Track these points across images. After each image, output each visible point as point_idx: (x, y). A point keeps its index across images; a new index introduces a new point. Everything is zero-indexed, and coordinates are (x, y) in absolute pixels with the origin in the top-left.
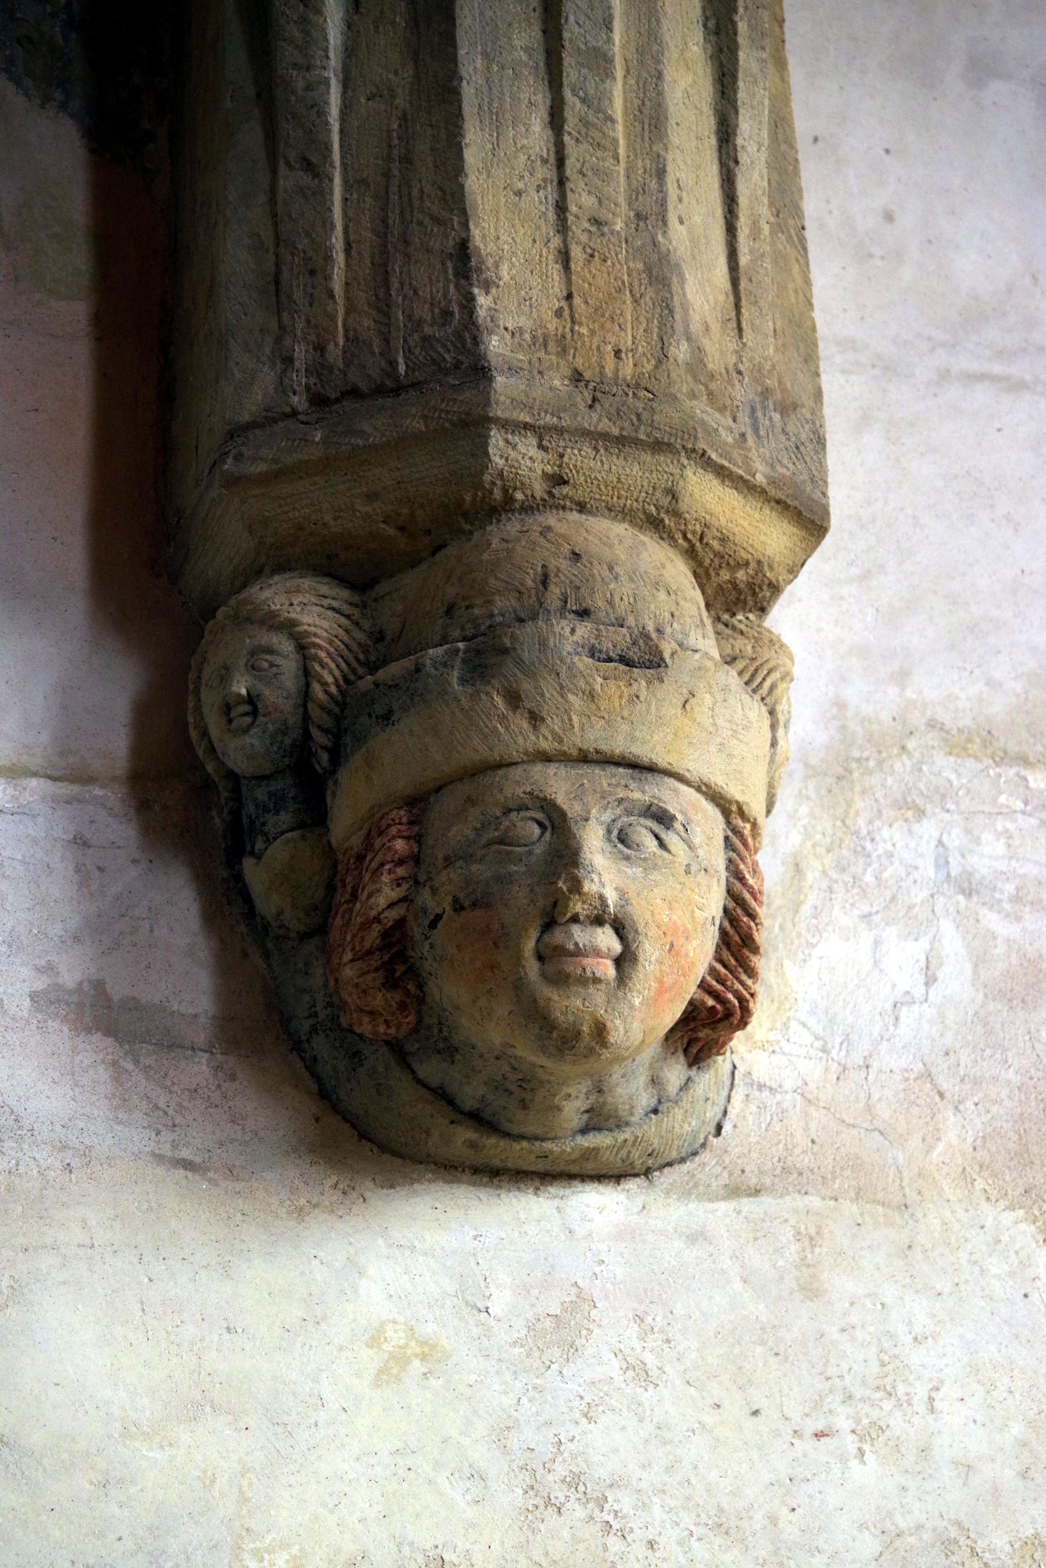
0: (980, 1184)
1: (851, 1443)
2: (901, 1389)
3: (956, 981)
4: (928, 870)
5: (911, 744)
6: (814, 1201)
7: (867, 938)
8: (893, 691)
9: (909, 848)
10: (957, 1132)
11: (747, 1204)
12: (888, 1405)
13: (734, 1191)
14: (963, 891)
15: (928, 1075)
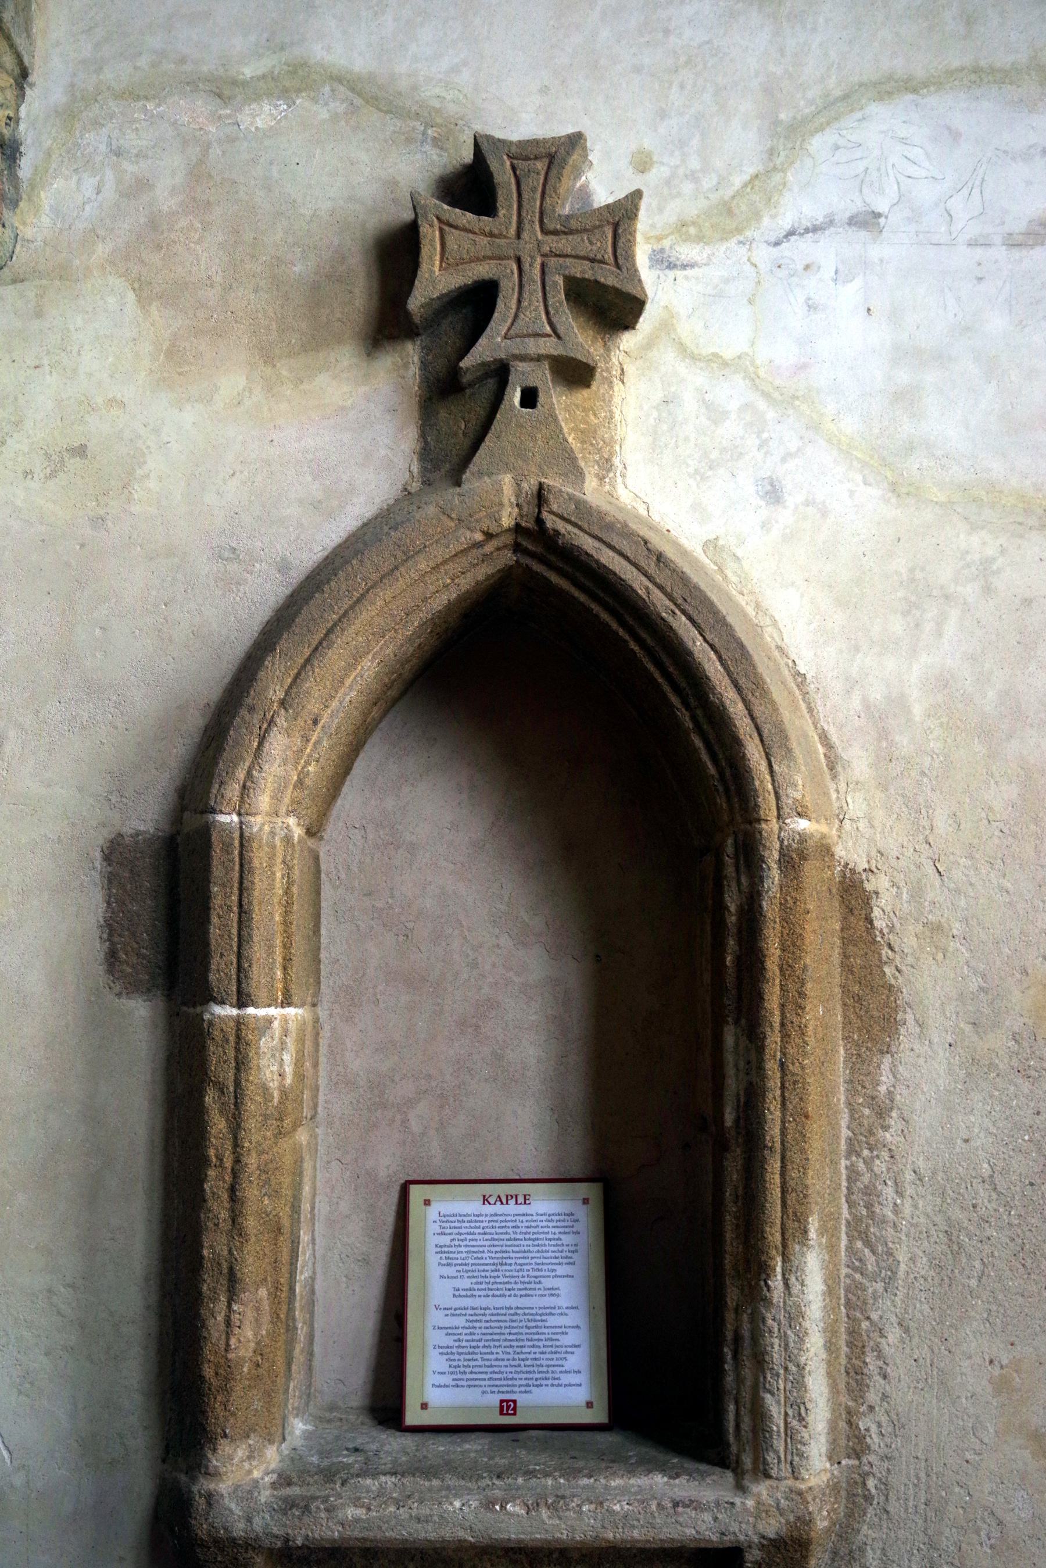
0: (108, 269)
1: (47, 368)
2: (69, 348)
3: (109, 193)
4: (103, 148)
5: (99, 98)
6: (44, 282)
7: (75, 178)
8: (95, 76)
9: (95, 141)
10: (102, 250)
11: (19, 285)
12: (63, 354)
13: (14, 281)
14: (116, 155)
15: (93, 230)
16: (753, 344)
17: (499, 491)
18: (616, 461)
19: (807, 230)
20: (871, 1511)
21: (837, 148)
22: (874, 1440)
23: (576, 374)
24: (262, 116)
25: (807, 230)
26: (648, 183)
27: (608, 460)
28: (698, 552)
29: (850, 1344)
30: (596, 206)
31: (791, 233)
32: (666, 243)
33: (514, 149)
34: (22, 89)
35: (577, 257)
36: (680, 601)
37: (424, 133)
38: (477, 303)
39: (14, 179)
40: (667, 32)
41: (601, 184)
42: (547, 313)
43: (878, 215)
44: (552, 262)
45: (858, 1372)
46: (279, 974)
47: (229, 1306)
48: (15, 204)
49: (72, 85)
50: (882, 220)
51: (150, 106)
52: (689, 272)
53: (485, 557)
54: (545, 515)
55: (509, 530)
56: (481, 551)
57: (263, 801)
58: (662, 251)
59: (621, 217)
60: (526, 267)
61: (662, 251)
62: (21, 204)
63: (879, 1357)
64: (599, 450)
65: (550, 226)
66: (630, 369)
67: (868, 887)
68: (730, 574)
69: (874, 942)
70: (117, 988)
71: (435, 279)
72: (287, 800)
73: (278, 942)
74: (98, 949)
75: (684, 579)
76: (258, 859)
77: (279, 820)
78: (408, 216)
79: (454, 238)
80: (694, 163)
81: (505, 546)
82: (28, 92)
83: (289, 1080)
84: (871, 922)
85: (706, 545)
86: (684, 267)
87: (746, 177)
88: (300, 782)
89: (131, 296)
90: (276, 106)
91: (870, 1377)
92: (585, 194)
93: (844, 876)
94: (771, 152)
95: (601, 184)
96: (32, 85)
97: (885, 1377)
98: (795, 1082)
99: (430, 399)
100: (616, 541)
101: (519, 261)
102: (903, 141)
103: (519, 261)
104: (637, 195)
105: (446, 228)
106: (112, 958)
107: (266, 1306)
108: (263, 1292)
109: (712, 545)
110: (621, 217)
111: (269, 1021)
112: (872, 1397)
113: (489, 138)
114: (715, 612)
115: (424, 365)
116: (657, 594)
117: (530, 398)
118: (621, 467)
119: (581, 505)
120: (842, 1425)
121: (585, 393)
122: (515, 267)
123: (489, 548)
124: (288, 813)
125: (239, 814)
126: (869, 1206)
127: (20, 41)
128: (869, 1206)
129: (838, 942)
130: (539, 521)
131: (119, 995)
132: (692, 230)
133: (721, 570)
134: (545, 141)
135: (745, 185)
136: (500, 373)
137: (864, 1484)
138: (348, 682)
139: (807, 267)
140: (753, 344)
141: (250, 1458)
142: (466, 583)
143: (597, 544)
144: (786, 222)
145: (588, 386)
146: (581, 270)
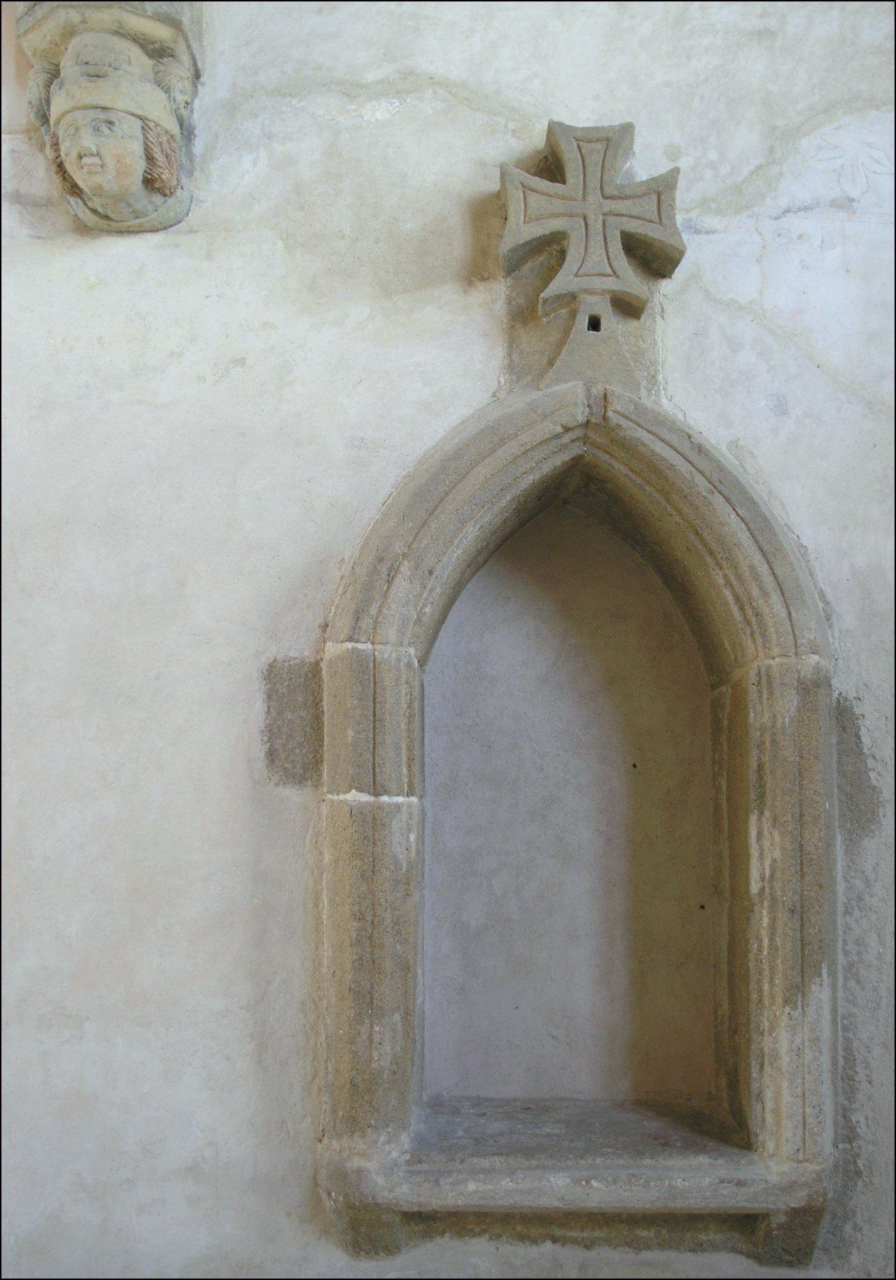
13: (190, 232)
16: (761, 293)
17: (568, 396)
18: (660, 377)
19: (799, 210)
20: (860, 1184)
21: (820, 148)
22: (862, 1130)
23: (629, 308)
24: (379, 111)
25: (799, 210)
26: (683, 163)
27: (653, 377)
28: (724, 449)
29: (845, 1058)
30: (638, 180)
31: (787, 211)
32: (694, 214)
33: (579, 134)
34: (195, 86)
35: (631, 217)
36: (717, 484)
37: (506, 126)
38: (551, 248)
39: (190, 154)
40: (689, 57)
41: (643, 164)
42: (608, 259)
43: (853, 200)
44: (610, 219)
45: (851, 1079)
46: (405, 771)
47: (372, 1027)
48: (191, 173)
49: (234, 84)
50: (855, 204)
51: (294, 101)
52: (712, 237)
53: (564, 447)
54: (610, 414)
55: (581, 425)
56: (559, 441)
57: (391, 632)
58: (690, 220)
59: (662, 189)
60: (590, 222)
61: (690, 220)
62: (196, 174)
63: (866, 1068)
64: (647, 368)
65: (609, 191)
66: (669, 308)
67: (857, 711)
68: (747, 466)
69: (861, 753)
70: (276, 779)
71: (520, 230)
72: (409, 634)
73: (404, 745)
74: (260, 752)
75: (720, 468)
76: (387, 679)
77: (402, 649)
78: (495, 186)
79: (534, 199)
80: (713, 155)
81: (577, 439)
82: (200, 88)
83: (413, 855)
84: (859, 738)
85: (730, 443)
86: (707, 233)
87: (752, 167)
88: (419, 620)
89: (280, 245)
90: (392, 104)
91: (860, 1082)
92: (630, 173)
93: (839, 702)
94: (771, 150)
95: (643, 164)
96: (203, 84)
97: (870, 1083)
98: (811, 860)
99: (512, 327)
100: (666, 434)
101: (585, 218)
102: (869, 145)
103: (585, 218)
104: (676, 171)
105: (528, 192)
106: (272, 755)
107: (399, 1026)
108: (397, 1017)
109: (734, 445)
110: (662, 189)
111: (398, 807)
112: (860, 1097)
113: (561, 125)
114: (744, 492)
115: (509, 301)
116: (699, 478)
117: (595, 324)
118: (663, 382)
119: (639, 408)
120: (841, 1119)
121: (635, 323)
122: (582, 222)
123: (566, 439)
124: (410, 645)
125: (373, 644)
126: (859, 953)
127: (194, 46)
128: (859, 953)
129: (835, 753)
130: (605, 418)
131: (277, 785)
132: (713, 206)
133: (742, 466)
134: (603, 128)
135: (752, 173)
136: (570, 299)
137: (855, 1163)
138: (456, 542)
139: (800, 237)
140: (761, 293)
141: (389, 1142)
142: (547, 468)
143: (652, 437)
144: (784, 202)
145: (638, 318)
146: (634, 227)
